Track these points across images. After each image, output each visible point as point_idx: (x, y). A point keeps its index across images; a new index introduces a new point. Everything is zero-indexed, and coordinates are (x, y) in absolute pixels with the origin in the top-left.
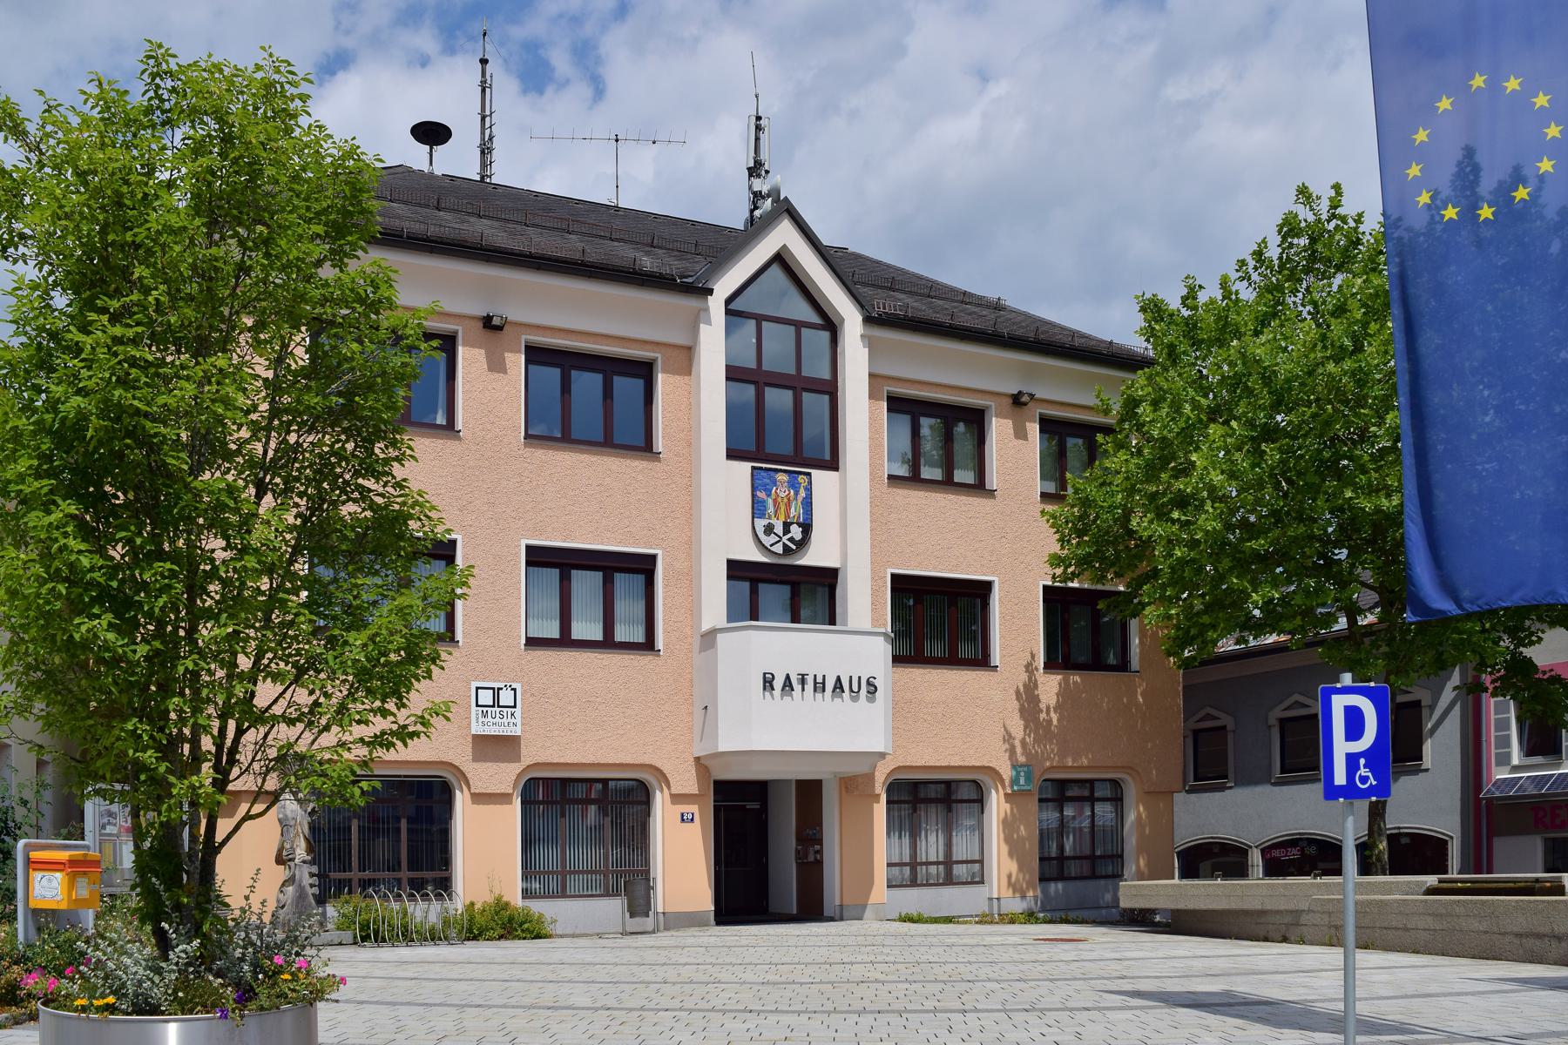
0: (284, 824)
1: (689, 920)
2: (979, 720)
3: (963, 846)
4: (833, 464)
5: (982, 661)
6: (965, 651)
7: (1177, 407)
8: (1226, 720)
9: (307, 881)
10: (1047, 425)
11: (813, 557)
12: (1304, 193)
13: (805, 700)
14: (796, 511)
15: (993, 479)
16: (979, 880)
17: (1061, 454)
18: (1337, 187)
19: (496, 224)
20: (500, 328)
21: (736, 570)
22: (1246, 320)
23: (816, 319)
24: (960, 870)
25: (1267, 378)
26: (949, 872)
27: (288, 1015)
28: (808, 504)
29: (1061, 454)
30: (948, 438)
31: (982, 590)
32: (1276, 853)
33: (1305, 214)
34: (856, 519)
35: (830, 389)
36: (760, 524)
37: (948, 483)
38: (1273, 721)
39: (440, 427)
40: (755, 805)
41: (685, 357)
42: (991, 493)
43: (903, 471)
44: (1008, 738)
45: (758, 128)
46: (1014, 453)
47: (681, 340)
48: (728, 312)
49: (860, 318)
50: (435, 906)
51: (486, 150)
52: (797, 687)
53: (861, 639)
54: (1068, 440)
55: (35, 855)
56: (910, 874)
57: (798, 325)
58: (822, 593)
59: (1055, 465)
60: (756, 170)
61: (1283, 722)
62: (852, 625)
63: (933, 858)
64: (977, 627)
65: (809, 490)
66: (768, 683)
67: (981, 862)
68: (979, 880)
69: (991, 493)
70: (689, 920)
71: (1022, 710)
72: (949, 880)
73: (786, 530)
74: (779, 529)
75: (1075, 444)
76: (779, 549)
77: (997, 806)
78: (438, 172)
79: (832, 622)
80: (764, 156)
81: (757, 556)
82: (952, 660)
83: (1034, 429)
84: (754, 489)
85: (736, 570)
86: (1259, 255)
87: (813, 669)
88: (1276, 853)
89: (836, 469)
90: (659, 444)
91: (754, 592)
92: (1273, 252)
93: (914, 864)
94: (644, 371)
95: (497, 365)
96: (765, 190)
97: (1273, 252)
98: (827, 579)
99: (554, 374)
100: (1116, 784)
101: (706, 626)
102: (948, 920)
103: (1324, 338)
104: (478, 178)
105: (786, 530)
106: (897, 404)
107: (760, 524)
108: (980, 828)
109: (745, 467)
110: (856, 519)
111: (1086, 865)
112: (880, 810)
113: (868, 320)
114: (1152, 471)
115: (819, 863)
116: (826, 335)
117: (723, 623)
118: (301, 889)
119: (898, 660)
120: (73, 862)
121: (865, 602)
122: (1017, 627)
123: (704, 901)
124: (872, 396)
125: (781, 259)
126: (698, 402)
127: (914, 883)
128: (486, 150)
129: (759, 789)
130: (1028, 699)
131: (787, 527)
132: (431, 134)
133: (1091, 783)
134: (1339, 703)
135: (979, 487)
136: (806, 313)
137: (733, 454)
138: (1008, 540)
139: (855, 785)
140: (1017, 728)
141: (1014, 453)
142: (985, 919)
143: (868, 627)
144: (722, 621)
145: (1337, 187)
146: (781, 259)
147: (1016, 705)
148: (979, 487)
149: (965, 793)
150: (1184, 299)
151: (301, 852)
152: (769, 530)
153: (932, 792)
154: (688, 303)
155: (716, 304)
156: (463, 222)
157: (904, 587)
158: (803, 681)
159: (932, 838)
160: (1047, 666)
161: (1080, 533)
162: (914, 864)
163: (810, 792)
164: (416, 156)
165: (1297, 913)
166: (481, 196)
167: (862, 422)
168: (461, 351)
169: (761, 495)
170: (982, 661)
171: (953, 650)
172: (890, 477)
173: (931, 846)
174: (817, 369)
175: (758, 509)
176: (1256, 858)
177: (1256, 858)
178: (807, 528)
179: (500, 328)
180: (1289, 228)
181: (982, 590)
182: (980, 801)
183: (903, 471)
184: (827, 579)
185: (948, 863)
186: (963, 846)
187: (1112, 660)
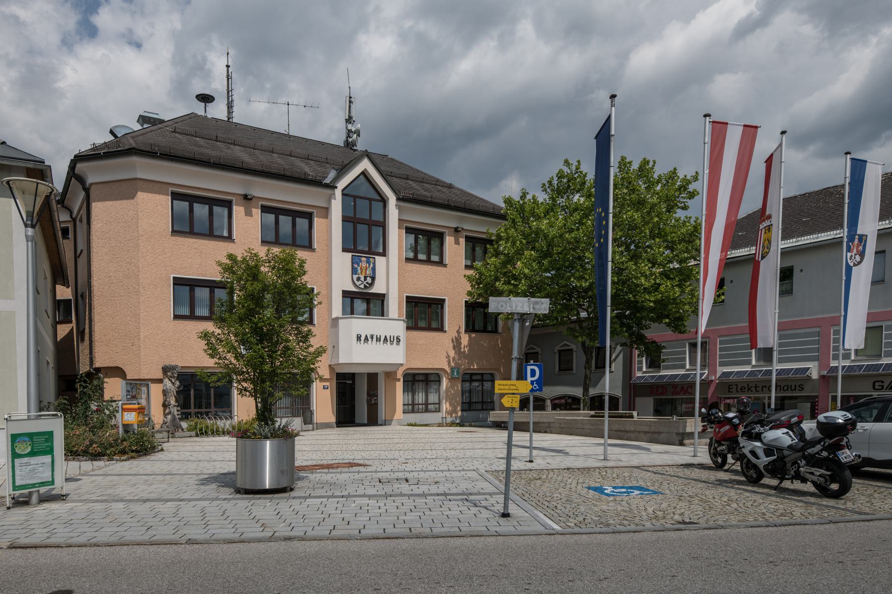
0: (165, 393)
1: (327, 426)
2: (438, 351)
3: (433, 398)
4: (384, 254)
5: (441, 329)
6: (434, 325)
7: (514, 243)
8: (538, 350)
9: (176, 413)
10: (468, 239)
11: (374, 290)
12: (566, 162)
13: (372, 345)
14: (369, 272)
15: (447, 260)
16: (438, 410)
17: (474, 250)
18: (579, 162)
19: (242, 149)
20: (251, 199)
21: (346, 294)
22: (540, 211)
23: (379, 198)
24: (431, 407)
25: (546, 236)
26: (413, 408)
27: (289, 440)
28: (374, 269)
29: (474, 250)
30: (429, 244)
31: (441, 302)
32: (556, 402)
33: (566, 170)
34: (392, 275)
35: (383, 225)
36: (355, 277)
37: (428, 261)
38: (556, 351)
39: (225, 237)
40: (350, 382)
41: (326, 212)
42: (445, 266)
43: (411, 255)
44: (448, 357)
45: (350, 102)
46: (455, 251)
47: (323, 204)
48: (343, 194)
49: (395, 198)
50: (228, 422)
51: (230, 106)
52: (370, 340)
53: (393, 324)
54: (477, 246)
55: (125, 407)
56: (411, 408)
57: (370, 200)
58: (379, 303)
59: (471, 255)
60: (349, 120)
61: (560, 351)
62: (390, 317)
63: (420, 402)
64: (439, 311)
65: (374, 264)
66: (359, 338)
67: (439, 404)
68: (438, 410)
69: (445, 266)
70: (327, 426)
71: (454, 347)
72: (427, 410)
73: (365, 279)
74: (362, 279)
75: (479, 250)
76: (362, 286)
77: (445, 382)
78: (209, 116)
79: (383, 315)
80: (353, 114)
81: (353, 289)
82: (429, 329)
83: (462, 241)
84: (353, 263)
85: (346, 294)
86: (550, 182)
87: (376, 333)
88: (556, 402)
89: (385, 256)
90: (315, 245)
91: (352, 303)
92: (555, 182)
93: (413, 404)
94: (309, 216)
95: (249, 213)
96: (353, 130)
97: (555, 182)
98: (381, 298)
99: (271, 217)
100: (492, 375)
101: (334, 316)
102: (426, 425)
103: (565, 225)
104: (226, 119)
105: (365, 279)
106: (409, 230)
107: (355, 277)
108: (438, 391)
109: (350, 255)
110: (392, 275)
111: (480, 405)
112: (399, 386)
113: (398, 199)
114: (504, 264)
115: (376, 404)
116: (381, 204)
117: (340, 315)
118: (174, 416)
119: (408, 328)
120: (139, 409)
121: (395, 306)
122: (454, 316)
123: (332, 419)
124: (399, 228)
125: (364, 174)
126: (331, 229)
127: (413, 411)
128: (230, 106)
129: (352, 376)
130: (457, 343)
131: (365, 278)
132: (205, 99)
133: (482, 374)
134: (529, 368)
135: (441, 263)
136: (373, 195)
137: (345, 250)
138: (451, 280)
139: (390, 375)
140: (452, 353)
141: (455, 251)
142: (440, 425)
143: (396, 317)
144: (340, 315)
145: (579, 162)
146: (364, 174)
147: (452, 345)
148: (441, 263)
149: (432, 378)
150: (521, 197)
151: (173, 401)
152: (358, 279)
153: (421, 378)
154: (329, 191)
155: (338, 193)
156: (229, 148)
157: (410, 300)
158: (372, 337)
159: (420, 394)
160: (466, 331)
161: (478, 284)
162: (413, 404)
163: (372, 378)
164: (199, 109)
165: (549, 423)
166: (229, 131)
167: (395, 238)
168: (235, 208)
169: (355, 266)
170: (441, 329)
171: (430, 324)
172: (406, 259)
173: (420, 398)
174: (377, 217)
175: (354, 271)
176: (548, 403)
177: (548, 403)
178: (373, 279)
179: (251, 199)
180: (560, 175)
181: (441, 302)
182: (439, 381)
183: (411, 255)
184: (381, 298)
185: (427, 404)
186: (433, 398)
187: (490, 329)
